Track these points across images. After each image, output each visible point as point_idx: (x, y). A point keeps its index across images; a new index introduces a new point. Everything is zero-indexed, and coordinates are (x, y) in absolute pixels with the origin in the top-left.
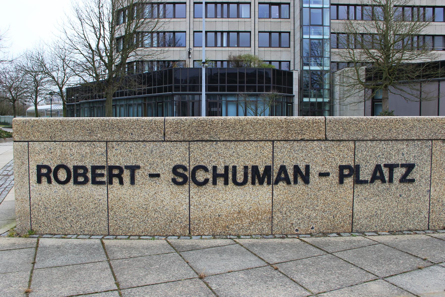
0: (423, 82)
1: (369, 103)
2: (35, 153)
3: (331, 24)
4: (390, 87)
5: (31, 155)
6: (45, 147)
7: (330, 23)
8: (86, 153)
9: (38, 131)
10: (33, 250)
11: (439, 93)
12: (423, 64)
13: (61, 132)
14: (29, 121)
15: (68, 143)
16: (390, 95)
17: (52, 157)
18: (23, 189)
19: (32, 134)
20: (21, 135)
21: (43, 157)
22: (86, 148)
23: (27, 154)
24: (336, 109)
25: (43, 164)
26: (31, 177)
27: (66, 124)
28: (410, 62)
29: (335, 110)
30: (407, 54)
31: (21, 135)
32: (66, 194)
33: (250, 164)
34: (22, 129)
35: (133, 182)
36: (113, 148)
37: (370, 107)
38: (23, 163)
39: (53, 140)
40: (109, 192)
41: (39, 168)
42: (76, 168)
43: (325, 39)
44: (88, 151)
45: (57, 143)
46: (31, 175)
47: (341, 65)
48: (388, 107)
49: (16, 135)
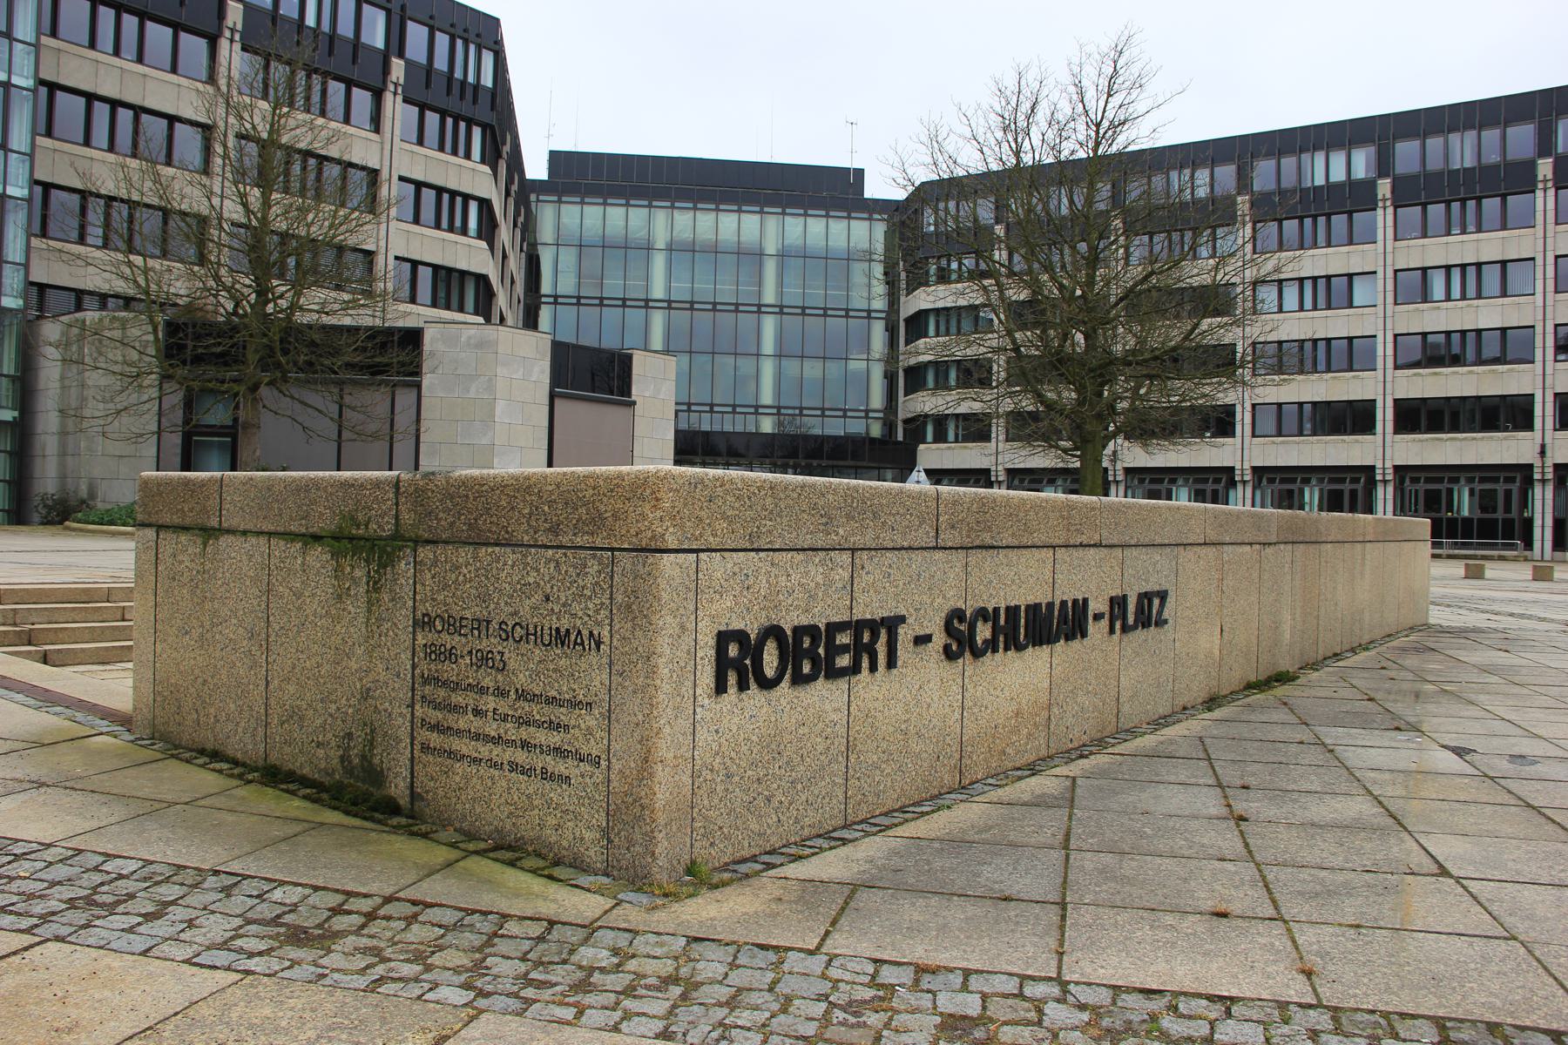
0: (355, 383)
1: (174, 440)
2: (712, 591)
3: (37, 150)
4: (264, 391)
5: (703, 598)
6: (736, 569)
7: (33, 144)
8: (817, 584)
9: (724, 517)
10: (1057, 856)
11: (418, 420)
12: (357, 329)
13: (771, 520)
14: (702, 481)
15: (784, 554)
16: (266, 418)
17: (750, 601)
18: (680, 721)
19: (709, 524)
20: (682, 527)
21: (729, 604)
22: (813, 571)
23: (691, 595)
24: (44, 450)
25: (730, 628)
26: (698, 673)
27: (783, 496)
28: (326, 320)
29: (38, 450)
30: (315, 297)
31: (682, 527)
32: (773, 719)
33: (1069, 598)
34: (685, 505)
35: (891, 663)
36: (863, 568)
37: (179, 451)
38: (683, 627)
39: (755, 546)
40: (852, 698)
41: (723, 638)
42: (799, 631)
43: (10, 197)
44: (820, 579)
45: (762, 554)
46: (699, 667)
47: (111, 302)
48: (258, 453)
49: (671, 530)
